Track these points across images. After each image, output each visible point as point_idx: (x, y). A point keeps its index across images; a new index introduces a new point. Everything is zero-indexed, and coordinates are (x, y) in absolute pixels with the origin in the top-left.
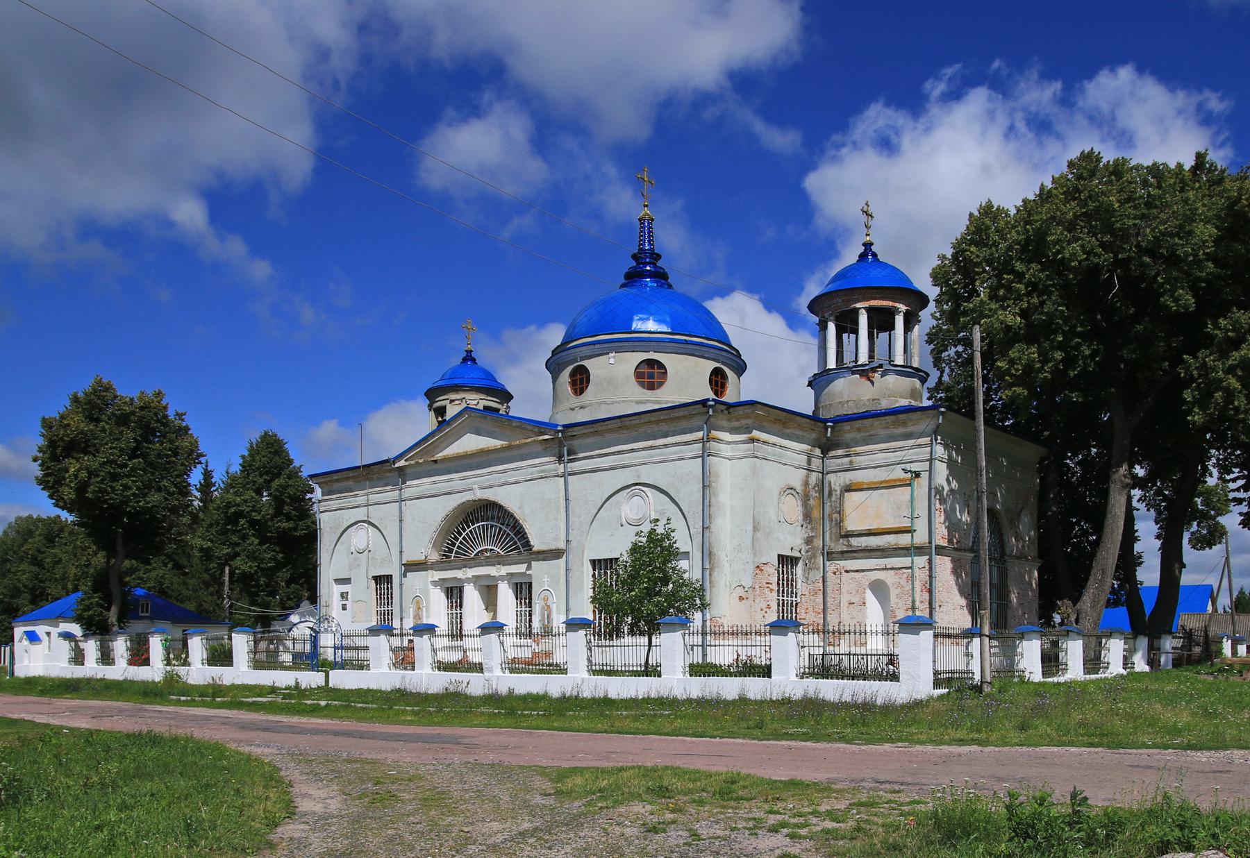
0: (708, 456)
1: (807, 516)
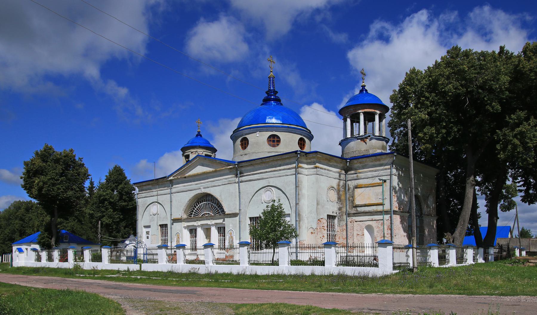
0: (298, 174)
1: (339, 198)
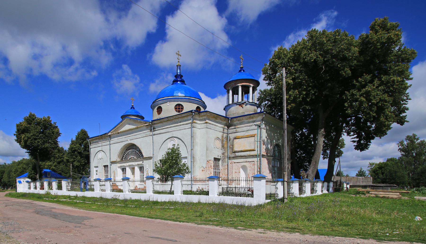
0: (193, 128)
1: (223, 146)
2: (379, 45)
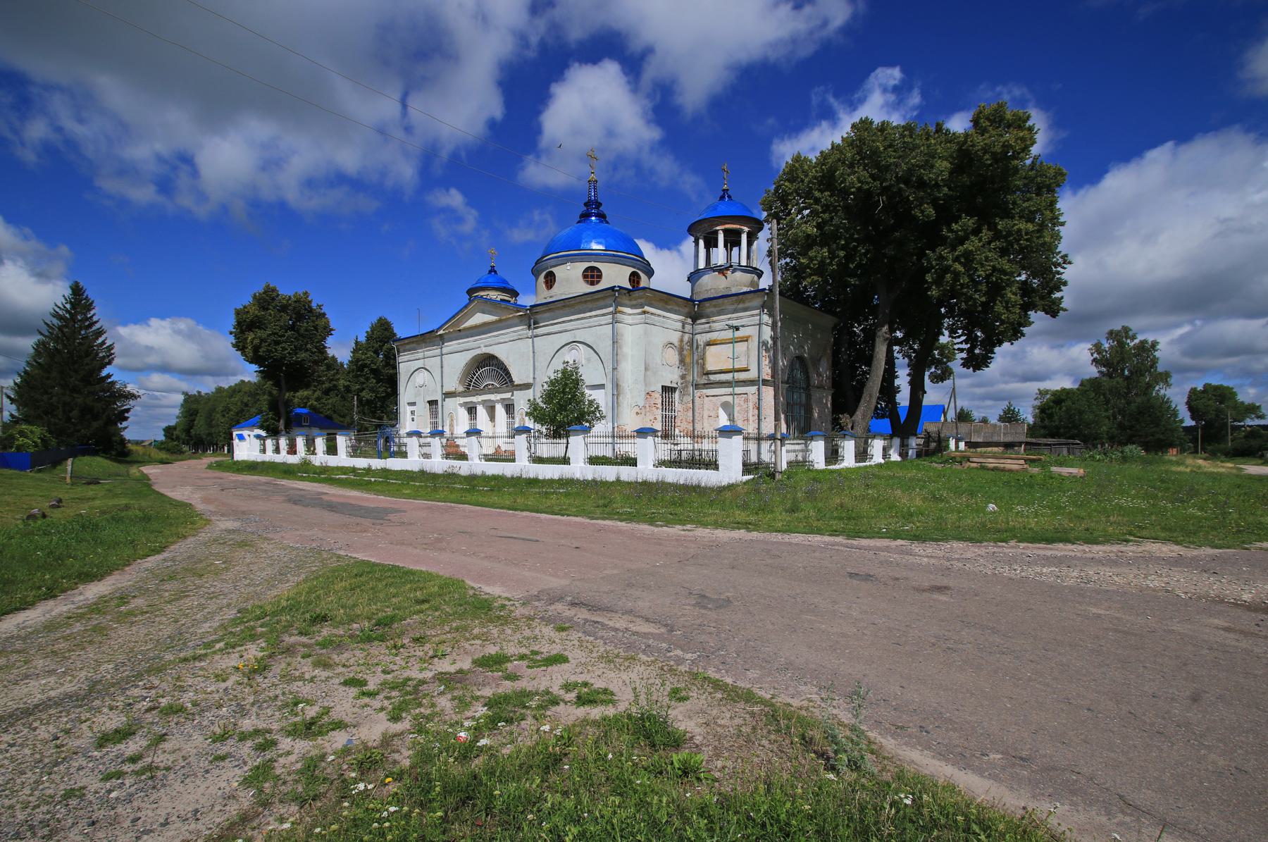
1: (682, 361)
2: (987, 158)
